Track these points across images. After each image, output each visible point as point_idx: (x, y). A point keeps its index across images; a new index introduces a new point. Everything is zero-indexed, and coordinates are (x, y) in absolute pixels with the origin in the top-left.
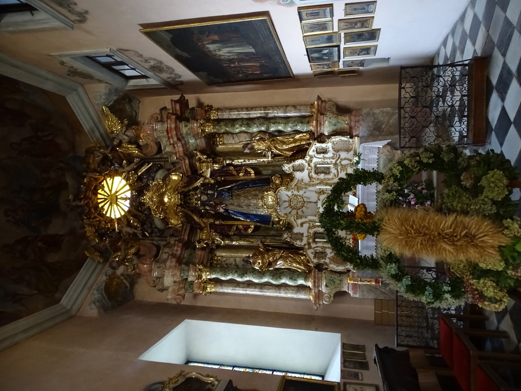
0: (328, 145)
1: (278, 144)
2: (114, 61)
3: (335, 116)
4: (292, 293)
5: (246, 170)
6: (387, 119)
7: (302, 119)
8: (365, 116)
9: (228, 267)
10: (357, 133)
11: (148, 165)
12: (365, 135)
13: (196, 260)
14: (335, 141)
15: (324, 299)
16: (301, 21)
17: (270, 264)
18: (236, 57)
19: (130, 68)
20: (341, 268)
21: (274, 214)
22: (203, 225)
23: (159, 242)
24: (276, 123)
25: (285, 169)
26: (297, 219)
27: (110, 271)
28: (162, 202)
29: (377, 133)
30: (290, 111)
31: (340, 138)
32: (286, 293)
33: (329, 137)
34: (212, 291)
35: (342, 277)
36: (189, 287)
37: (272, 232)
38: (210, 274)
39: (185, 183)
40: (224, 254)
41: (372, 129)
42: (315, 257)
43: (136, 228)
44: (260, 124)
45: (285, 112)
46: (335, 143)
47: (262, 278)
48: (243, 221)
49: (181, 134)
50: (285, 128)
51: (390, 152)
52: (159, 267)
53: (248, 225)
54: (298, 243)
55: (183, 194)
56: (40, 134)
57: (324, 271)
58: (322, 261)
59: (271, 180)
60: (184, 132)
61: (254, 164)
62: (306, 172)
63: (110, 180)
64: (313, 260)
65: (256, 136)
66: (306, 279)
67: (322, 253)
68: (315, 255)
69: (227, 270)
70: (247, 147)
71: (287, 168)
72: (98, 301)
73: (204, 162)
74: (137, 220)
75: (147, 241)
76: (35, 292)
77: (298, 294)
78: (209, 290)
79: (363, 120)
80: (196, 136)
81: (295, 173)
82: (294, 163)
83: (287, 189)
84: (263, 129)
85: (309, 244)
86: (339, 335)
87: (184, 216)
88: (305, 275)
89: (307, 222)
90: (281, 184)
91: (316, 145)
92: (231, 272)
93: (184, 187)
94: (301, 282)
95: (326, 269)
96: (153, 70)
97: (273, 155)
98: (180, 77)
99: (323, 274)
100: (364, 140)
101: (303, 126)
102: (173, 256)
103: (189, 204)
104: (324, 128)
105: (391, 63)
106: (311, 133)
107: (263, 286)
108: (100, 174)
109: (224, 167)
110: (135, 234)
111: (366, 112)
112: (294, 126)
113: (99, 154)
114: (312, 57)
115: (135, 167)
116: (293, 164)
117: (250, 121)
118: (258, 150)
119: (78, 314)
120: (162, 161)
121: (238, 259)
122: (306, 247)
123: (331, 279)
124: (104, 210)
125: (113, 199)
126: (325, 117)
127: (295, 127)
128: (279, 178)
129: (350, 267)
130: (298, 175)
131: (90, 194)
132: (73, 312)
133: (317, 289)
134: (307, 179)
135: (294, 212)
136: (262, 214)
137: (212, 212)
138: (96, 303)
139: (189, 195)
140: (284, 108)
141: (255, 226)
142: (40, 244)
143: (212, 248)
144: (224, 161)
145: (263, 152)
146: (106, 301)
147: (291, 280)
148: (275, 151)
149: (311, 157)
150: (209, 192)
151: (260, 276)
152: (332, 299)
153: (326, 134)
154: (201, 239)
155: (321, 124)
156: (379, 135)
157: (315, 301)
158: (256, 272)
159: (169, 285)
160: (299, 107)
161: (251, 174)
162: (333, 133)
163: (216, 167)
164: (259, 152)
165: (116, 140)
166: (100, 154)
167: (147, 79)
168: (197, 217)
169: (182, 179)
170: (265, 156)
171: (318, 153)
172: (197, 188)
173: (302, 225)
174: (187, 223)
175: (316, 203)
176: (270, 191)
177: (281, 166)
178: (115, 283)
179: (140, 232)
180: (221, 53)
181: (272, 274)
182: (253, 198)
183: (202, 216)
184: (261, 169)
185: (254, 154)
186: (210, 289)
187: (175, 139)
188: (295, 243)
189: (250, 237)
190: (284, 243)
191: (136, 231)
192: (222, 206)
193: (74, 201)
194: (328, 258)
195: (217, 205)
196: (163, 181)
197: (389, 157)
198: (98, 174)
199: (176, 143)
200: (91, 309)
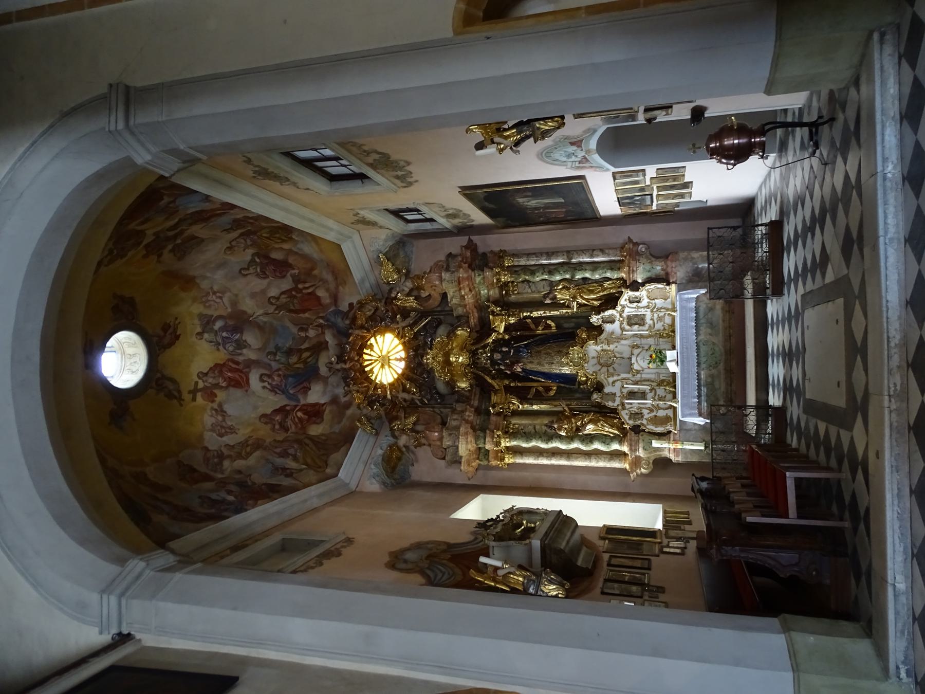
0: (643, 293)
1: (585, 292)
7: (613, 265)
10: (674, 280)
12: (684, 281)
16: (614, 181)
17: (578, 429)
18: (542, 206)
20: (660, 430)
21: (581, 373)
22: (497, 387)
23: (442, 410)
26: (608, 377)
27: (391, 440)
28: (447, 363)
29: (696, 279)
30: (598, 256)
33: (643, 284)
34: (510, 462)
37: (578, 395)
38: (510, 441)
39: (474, 340)
42: (630, 419)
44: (564, 272)
45: (592, 256)
46: (650, 290)
50: (592, 275)
52: (450, 435)
54: (610, 404)
56: (300, 286)
58: (638, 423)
62: (617, 323)
65: (558, 285)
66: (621, 442)
67: (637, 414)
70: (548, 297)
71: (595, 319)
72: (378, 476)
73: (497, 315)
74: (413, 385)
75: (427, 409)
76: (304, 467)
77: (612, 462)
78: (506, 461)
79: (680, 265)
80: (491, 286)
81: (605, 325)
83: (596, 344)
84: (568, 276)
85: (623, 404)
86: (661, 505)
87: (474, 378)
88: (620, 439)
90: (589, 338)
91: (628, 294)
93: (473, 344)
94: (615, 446)
96: (447, 218)
98: (473, 221)
100: (682, 288)
103: (477, 363)
105: (709, 204)
108: (368, 331)
111: (684, 256)
113: (370, 308)
114: (623, 203)
115: (411, 322)
117: (551, 269)
118: (561, 300)
119: (357, 489)
120: (442, 315)
122: (620, 408)
124: (373, 373)
125: (385, 361)
130: (608, 327)
131: (353, 354)
132: (353, 486)
134: (618, 331)
135: (605, 369)
139: (478, 354)
140: (590, 252)
142: (300, 414)
145: (565, 302)
147: (603, 444)
149: (623, 307)
150: (504, 349)
153: (640, 281)
155: (633, 271)
161: (552, 327)
163: (512, 320)
168: (490, 378)
170: (568, 307)
171: (631, 302)
173: (614, 382)
174: (477, 386)
175: (630, 359)
176: (576, 346)
180: (529, 204)
182: (555, 355)
184: (562, 321)
185: (556, 305)
186: (509, 460)
188: (607, 404)
190: (593, 406)
191: (414, 397)
192: (520, 365)
193: (337, 363)
194: (646, 419)
195: (513, 364)
196: (447, 338)
197: (709, 305)
199: (467, 295)
200: (372, 484)
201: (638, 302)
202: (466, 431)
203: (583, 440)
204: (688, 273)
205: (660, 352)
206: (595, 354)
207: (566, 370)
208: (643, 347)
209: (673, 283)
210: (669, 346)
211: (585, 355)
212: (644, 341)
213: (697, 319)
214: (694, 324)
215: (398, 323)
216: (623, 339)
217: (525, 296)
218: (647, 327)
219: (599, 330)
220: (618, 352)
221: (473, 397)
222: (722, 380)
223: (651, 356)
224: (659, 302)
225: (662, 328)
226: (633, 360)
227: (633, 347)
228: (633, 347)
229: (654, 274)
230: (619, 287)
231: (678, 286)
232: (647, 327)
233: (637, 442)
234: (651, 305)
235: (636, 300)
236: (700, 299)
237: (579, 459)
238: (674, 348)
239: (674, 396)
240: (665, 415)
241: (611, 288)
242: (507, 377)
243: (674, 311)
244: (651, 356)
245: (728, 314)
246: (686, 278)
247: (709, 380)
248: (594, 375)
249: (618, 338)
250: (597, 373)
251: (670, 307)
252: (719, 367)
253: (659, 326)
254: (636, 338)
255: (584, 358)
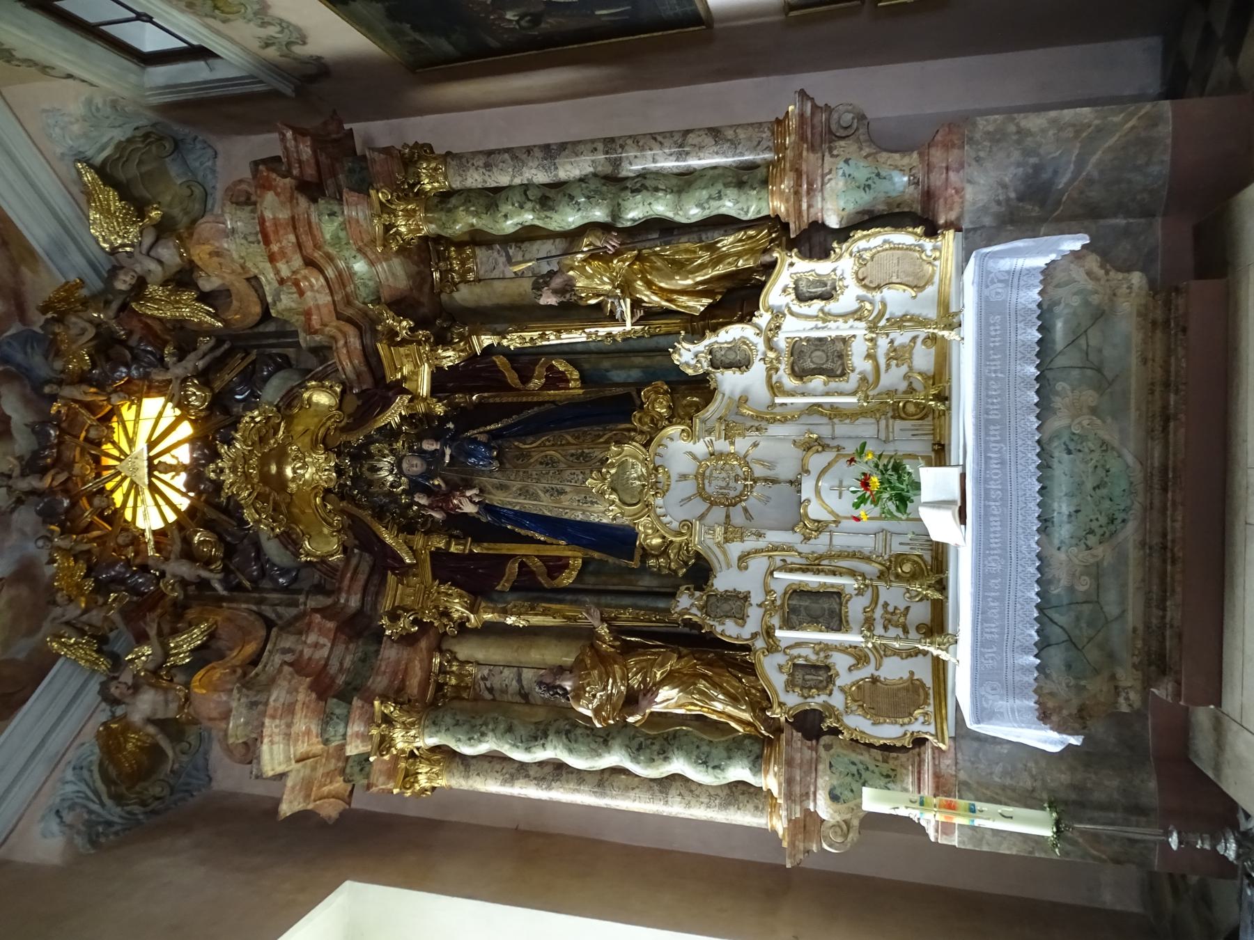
1: (658, 269)
2: (185, 45)
3: (866, 151)
4: (709, 806)
5: (551, 368)
6: (1076, 152)
8: (987, 144)
9: (494, 700)
10: (952, 216)
11: (243, 359)
13: (379, 679)
14: (865, 250)
15: (826, 838)
17: (632, 700)
19: (133, 15)
20: (888, 732)
24: (646, 188)
25: (683, 360)
26: (727, 540)
31: (887, 237)
32: (688, 805)
33: (843, 234)
35: (892, 764)
36: (357, 769)
38: (421, 734)
40: (480, 655)
41: (1013, 195)
42: (790, 685)
43: (207, 562)
46: (867, 255)
47: (599, 755)
48: (544, 543)
49: (317, 246)
50: (677, 207)
51: (1097, 279)
53: (559, 558)
54: (729, 630)
55: (349, 454)
57: (825, 739)
59: (638, 403)
60: (328, 237)
61: (579, 348)
62: (758, 369)
63: (129, 408)
64: (783, 697)
66: (758, 763)
67: (815, 668)
68: (791, 675)
69: (479, 722)
70: (547, 284)
72: (71, 808)
73: (404, 342)
75: (244, 606)
78: (423, 781)
82: (713, 339)
83: (691, 435)
85: (769, 632)
89: (762, 551)
92: (493, 730)
95: (835, 732)
97: (640, 314)
99: (821, 750)
101: (743, 198)
102: (299, 667)
103: (370, 483)
104: (823, 199)
106: (774, 223)
107: (606, 776)
109: (473, 358)
110: (204, 584)
112: (710, 198)
113: (83, 324)
115: (201, 364)
116: (710, 339)
118: (588, 298)
121: (528, 675)
122: (760, 644)
123: (853, 769)
126: (827, 158)
127: (714, 204)
128: (666, 392)
129: (925, 729)
130: (729, 382)
133: (798, 808)
134: (760, 392)
135: (718, 513)
136: (605, 521)
137: (434, 514)
138: (64, 813)
141: (586, 562)
143: (445, 633)
144: (474, 338)
146: (102, 804)
147: (702, 768)
148: (651, 299)
149: (778, 314)
151: (593, 746)
152: (853, 836)
153: (833, 222)
154: (399, 607)
155: (810, 191)
156: (1041, 220)
157: (792, 844)
158: (579, 731)
159: (280, 769)
160: (730, 134)
161: (568, 381)
162: (858, 219)
163: (449, 357)
164: (593, 302)
165: (122, 277)
166: (87, 325)
167: (210, 61)
169: (341, 401)
170: (612, 318)
171: (802, 298)
172: (390, 434)
173: (744, 557)
175: (796, 483)
177: (665, 352)
178: (130, 746)
179: (219, 576)
181: (635, 743)
183: (408, 527)
187: (297, 262)
188: (719, 629)
189: (569, 597)
192: (468, 493)
193: (23, 475)
194: (842, 689)
197: (1095, 299)
198: (93, 390)
201: (827, 297)
202: (289, 699)
203: (640, 748)
204: (1004, 186)
205: (898, 468)
206: (688, 466)
207: (607, 512)
208: (839, 448)
209: (948, 226)
210: (922, 446)
211: (656, 469)
212: (842, 429)
213: (1044, 347)
214: (1032, 371)
215: (166, 368)
216: (775, 421)
217: (499, 286)
218: (853, 380)
219: (702, 388)
220: (760, 461)
221: (346, 582)
222: (1131, 587)
223: (865, 484)
224: (897, 299)
225: (903, 386)
226: (807, 490)
227: (808, 447)
228: (808, 447)
229: (882, 196)
230: (766, 251)
231: (966, 238)
232: (853, 380)
233: (813, 766)
234: (868, 306)
235: (820, 290)
236: (1060, 276)
237: (632, 794)
238: (939, 455)
239: (937, 626)
240: (906, 676)
241: (739, 255)
242: (432, 529)
243: (950, 327)
244: (865, 484)
245: (1159, 334)
246: (995, 208)
247: (1084, 585)
248: (682, 534)
249: (759, 417)
250: (690, 528)
251: (932, 314)
252: (1121, 537)
253: (893, 378)
254: (816, 419)
255: (656, 482)
